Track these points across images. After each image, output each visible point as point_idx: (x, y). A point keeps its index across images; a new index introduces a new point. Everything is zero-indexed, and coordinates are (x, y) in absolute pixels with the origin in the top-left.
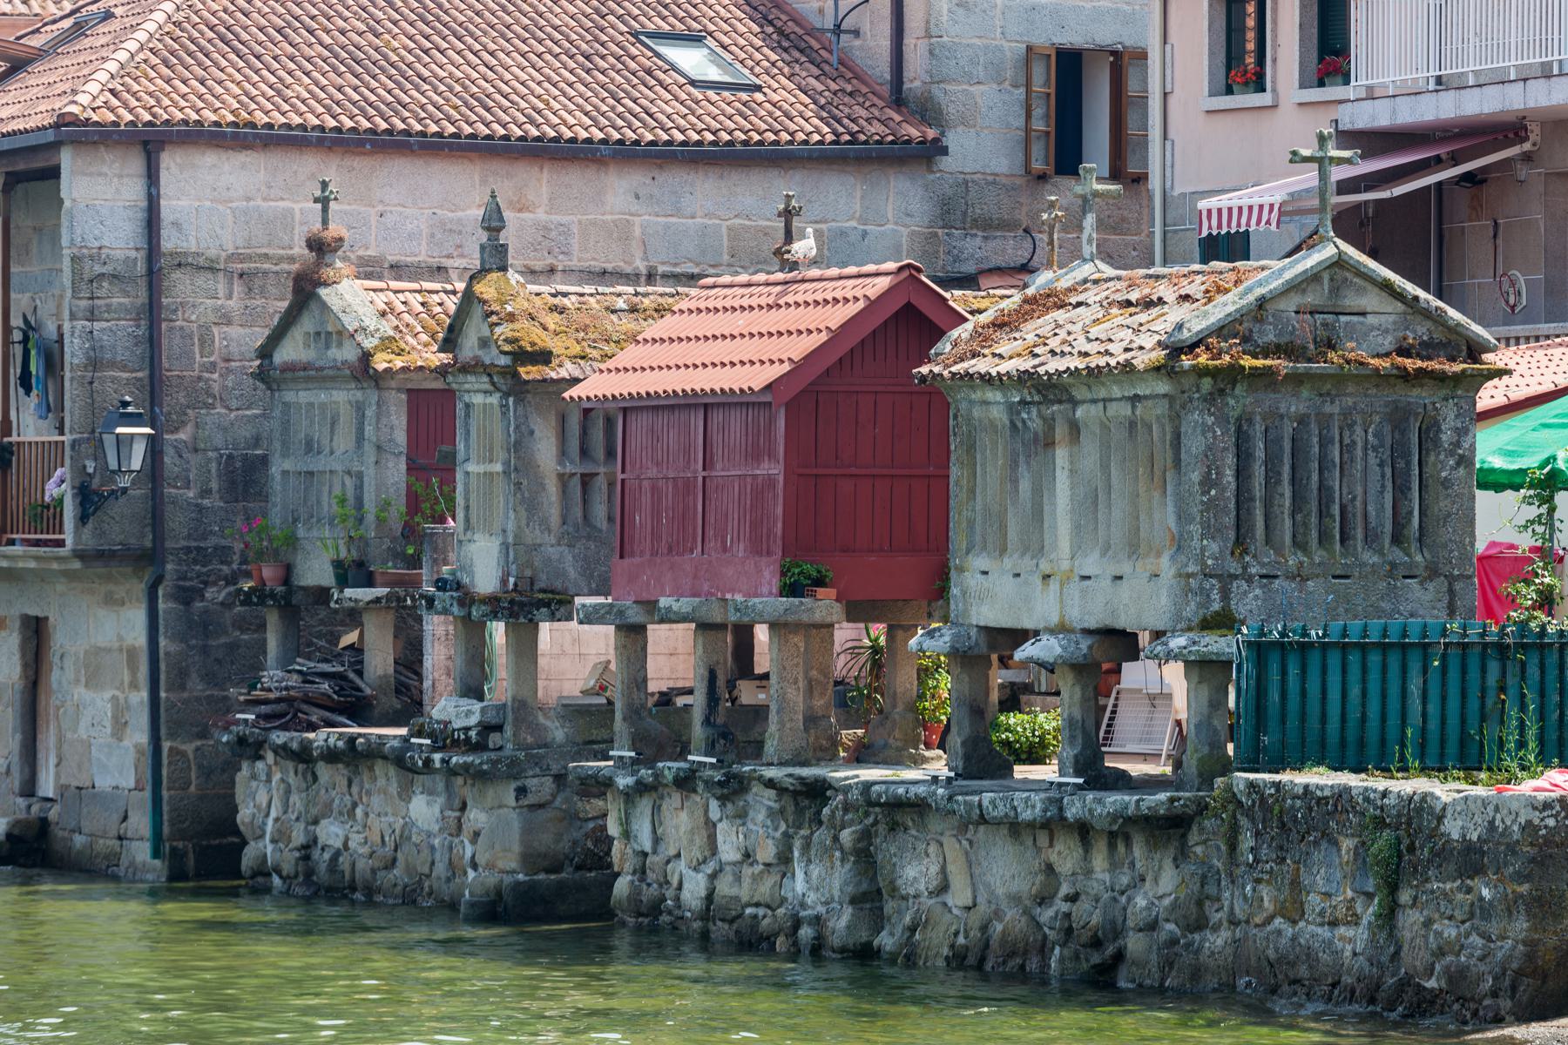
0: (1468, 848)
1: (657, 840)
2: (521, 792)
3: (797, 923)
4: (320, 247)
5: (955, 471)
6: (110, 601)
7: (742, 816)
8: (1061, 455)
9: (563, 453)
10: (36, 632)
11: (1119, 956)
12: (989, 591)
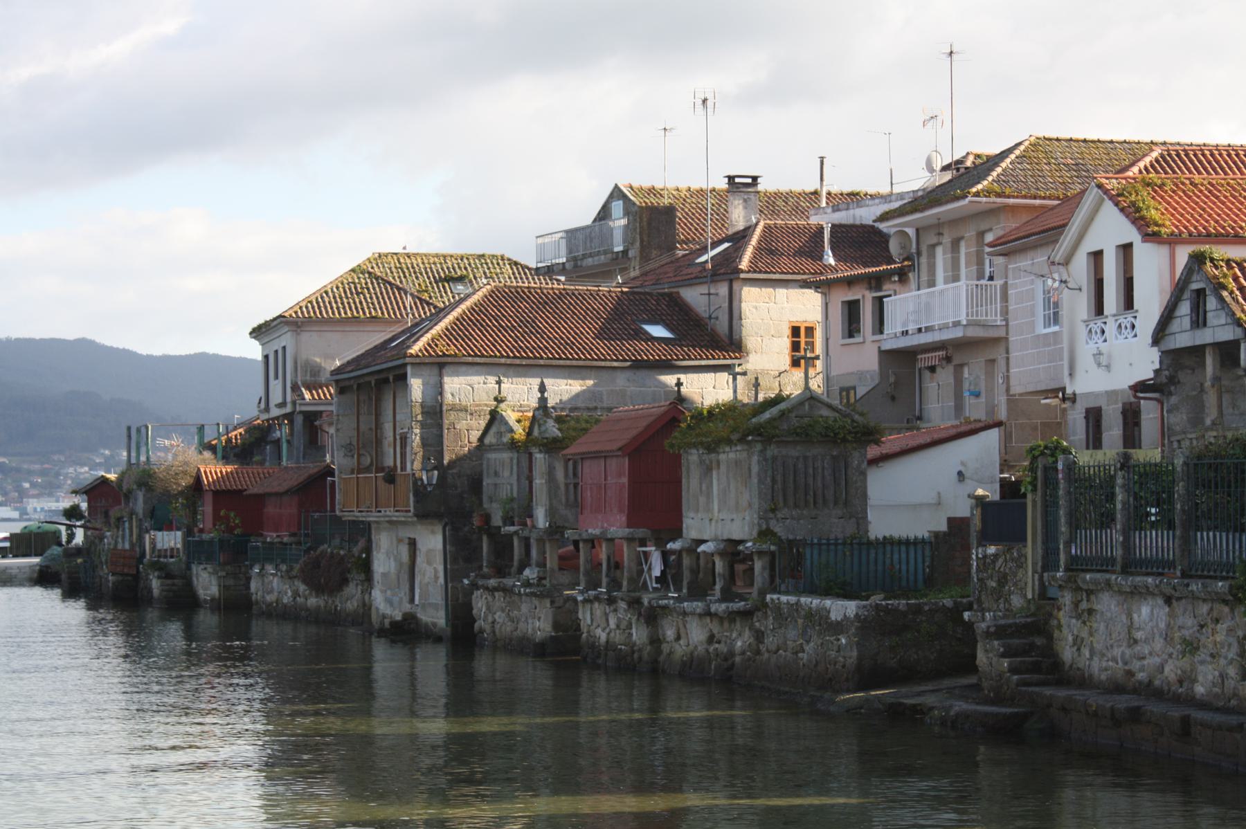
0: (838, 623)
1: (592, 620)
2: (552, 602)
3: (633, 652)
4: (499, 400)
5: (684, 481)
6: (433, 532)
7: (615, 610)
8: (714, 473)
9: (566, 475)
10: (413, 544)
11: (733, 664)
12: (693, 526)
